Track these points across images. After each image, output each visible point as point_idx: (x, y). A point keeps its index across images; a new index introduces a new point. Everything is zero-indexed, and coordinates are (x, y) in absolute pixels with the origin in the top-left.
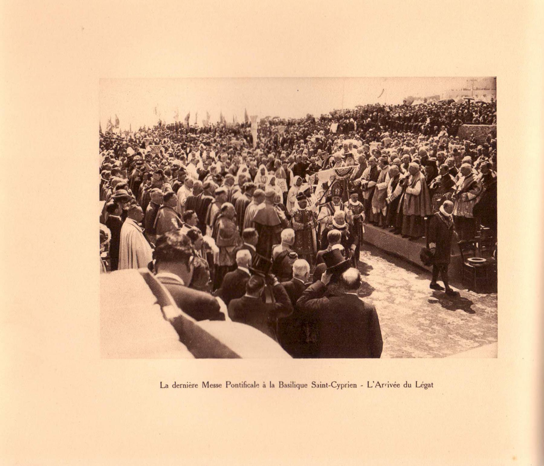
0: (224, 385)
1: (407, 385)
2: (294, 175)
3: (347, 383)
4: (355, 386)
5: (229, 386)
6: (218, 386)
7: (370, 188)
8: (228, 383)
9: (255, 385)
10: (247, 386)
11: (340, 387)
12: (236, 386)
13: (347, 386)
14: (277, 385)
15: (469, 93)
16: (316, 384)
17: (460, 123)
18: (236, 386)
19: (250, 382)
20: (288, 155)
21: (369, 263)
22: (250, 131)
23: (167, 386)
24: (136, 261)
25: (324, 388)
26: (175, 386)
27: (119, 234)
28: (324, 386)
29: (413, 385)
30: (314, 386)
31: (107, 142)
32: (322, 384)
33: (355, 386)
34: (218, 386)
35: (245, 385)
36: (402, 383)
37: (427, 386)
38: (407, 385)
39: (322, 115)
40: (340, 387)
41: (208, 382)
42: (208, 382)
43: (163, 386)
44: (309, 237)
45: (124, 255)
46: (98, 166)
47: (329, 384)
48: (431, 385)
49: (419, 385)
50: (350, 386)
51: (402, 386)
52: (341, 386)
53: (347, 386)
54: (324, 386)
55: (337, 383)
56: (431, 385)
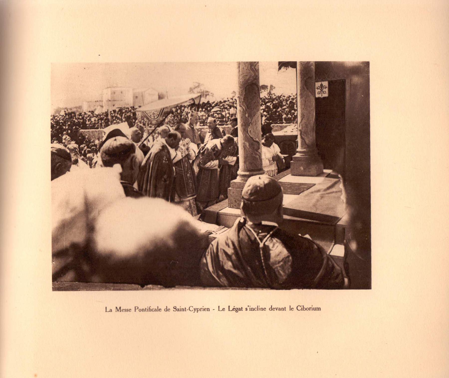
0: (133, 309)
1: (167, 310)
4: (208, 310)
5: (137, 310)
6: (129, 310)
8: (136, 308)
11: (196, 311)
12: (143, 310)
13: (202, 310)
15: (166, 98)
17: (78, 128)
18: (143, 310)
19: (154, 307)
20: (203, 116)
23: (111, 311)
25: (183, 312)
26: (272, 309)
28: (184, 310)
29: (227, 309)
30: (175, 310)
31: (258, 62)
33: (208, 310)
34: (129, 310)
35: (150, 310)
36: (163, 308)
38: (167, 310)
39: (363, 70)
40: (196, 311)
41: (120, 308)
42: (120, 308)
43: (108, 310)
47: (187, 308)
49: (231, 309)
50: (204, 310)
51: (163, 310)
52: (197, 310)
53: (202, 310)
54: (184, 310)
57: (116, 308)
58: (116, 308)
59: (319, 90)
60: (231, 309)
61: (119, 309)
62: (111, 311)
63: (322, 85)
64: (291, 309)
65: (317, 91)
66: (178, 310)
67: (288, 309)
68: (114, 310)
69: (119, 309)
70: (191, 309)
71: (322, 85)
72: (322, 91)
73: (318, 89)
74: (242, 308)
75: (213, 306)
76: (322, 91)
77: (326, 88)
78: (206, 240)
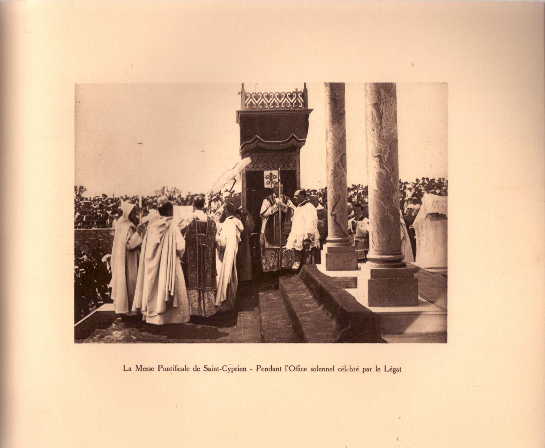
0: (283, 369)
1: (197, 369)
2: (350, 229)
4: (245, 370)
5: (161, 370)
6: (151, 369)
9: (186, 369)
10: (178, 370)
12: (168, 369)
14: (202, 368)
18: (168, 369)
19: (181, 366)
22: (180, 196)
23: (130, 369)
24: (167, 247)
28: (216, 369)
29: (383, 369)
30: (206, 369)
32: (213, 367)
33: (245, 370)
34: (151, 369)
35: (176, 369)
36: (192, 367)
37: (395, 371)
38: (197, 369)
41: (141, 366)
42: (141, 366)
43: (126, 368)
48: (399, 370)
49: (387, 369)
50: (240, 370)
51: (191, 369)
54: (216, 369)
56: (399, 370)
57: (137, 366)
58: (137, 366)
59: (269, 180)
60: (387, 369)
61: (140, 368)
62: (130, 369)
63: (271, 174)
64: (378, 370)
65: (266, 181)
66: (210, 370)
67: (374, 369)
68: (134, 368)
69: (140, 368)
70: (225, 368)
71: (271, 174)
72: (271, 181)
73: (267, 178)
74: (280, 368)
75: (250, 365)
76: (271, 181)
77: (276, 177)
78: (318, 261)
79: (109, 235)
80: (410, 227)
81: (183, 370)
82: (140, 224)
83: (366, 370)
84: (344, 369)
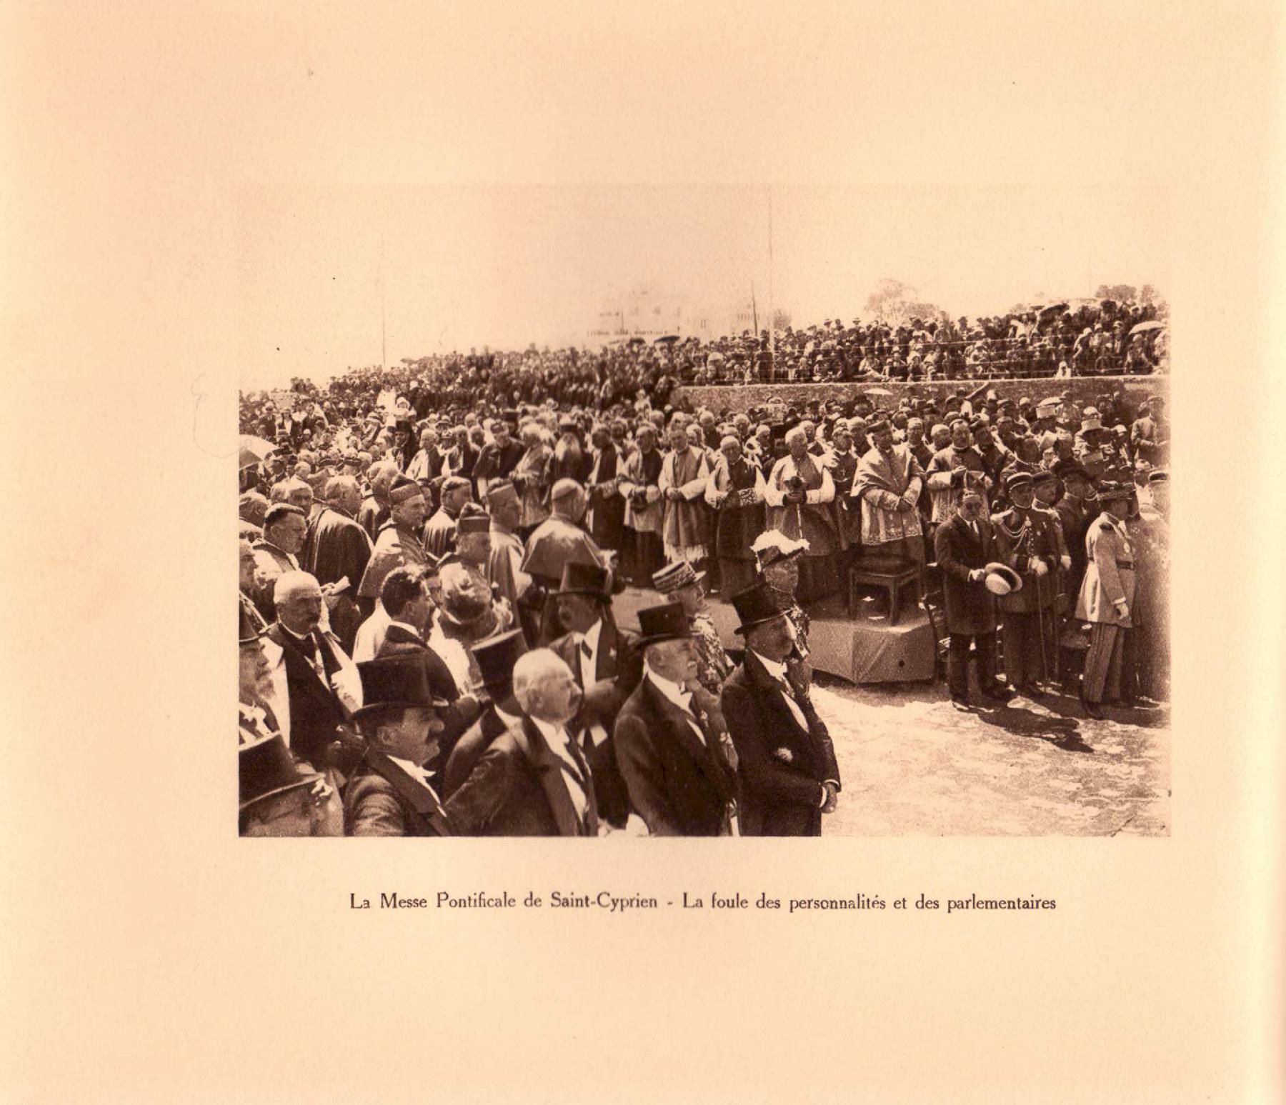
0: (432, 901)
3: (633, 895)
4: (653, 903)
5: (444, 904)
6: (420, 903)
7: (654, 503)
8: (443, 897)
9: (507, 901)
11: (619, 905)
12: (460, 903)
13: (635, 903)
16: (561, 897)
18: (460, 903)
19: (494, 893)
21: (602, 682)
25: (580, 909)
27: (355, 634)
30: (556, 902)
32: (575, 897)
33: (653, 903)
34: (420, 903)
35: (481, 901)
36: (520, 895)
38: (532, 901)
40: (619, 905)
41: (394, 895)
42: (394, 895)
43: (358, 902)
44: (855, 525)
45: (1138, 382)
46: (517, 350)
47: (593, 898)
50: (641, 903)
51: (520, 902)
53: (635, 903)
55: (612, 896)
61: (391, 901)
62: (700, 904)
63: (882, 499)
66: (566, 903)
69: (391, 901)
70: (604, 900)
74: (587, 899)
79: (840, 467)
80: (518, 692)
81: (499, 903)
82: (492, 526)
83: (799, 904)
84: (737, 903)
